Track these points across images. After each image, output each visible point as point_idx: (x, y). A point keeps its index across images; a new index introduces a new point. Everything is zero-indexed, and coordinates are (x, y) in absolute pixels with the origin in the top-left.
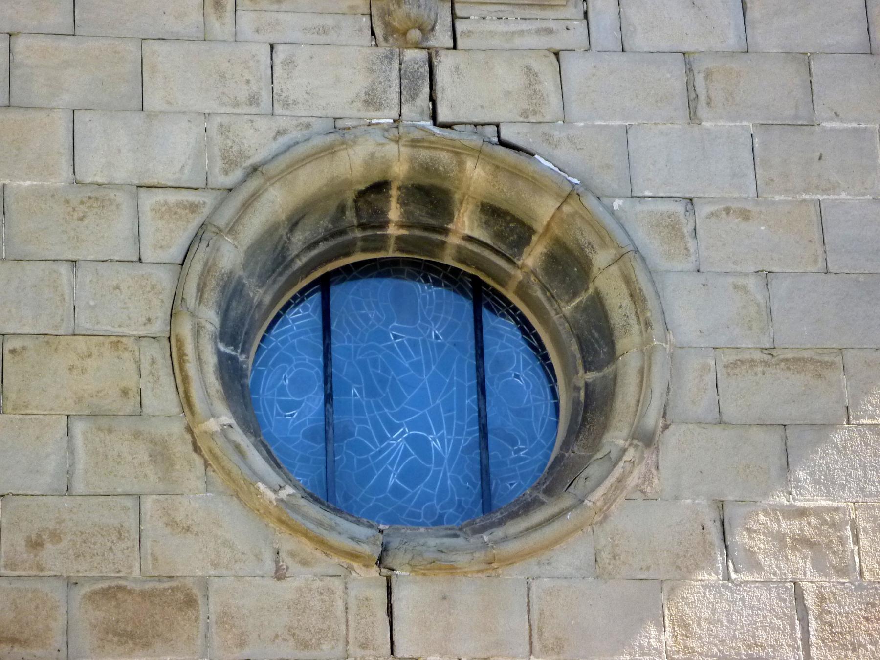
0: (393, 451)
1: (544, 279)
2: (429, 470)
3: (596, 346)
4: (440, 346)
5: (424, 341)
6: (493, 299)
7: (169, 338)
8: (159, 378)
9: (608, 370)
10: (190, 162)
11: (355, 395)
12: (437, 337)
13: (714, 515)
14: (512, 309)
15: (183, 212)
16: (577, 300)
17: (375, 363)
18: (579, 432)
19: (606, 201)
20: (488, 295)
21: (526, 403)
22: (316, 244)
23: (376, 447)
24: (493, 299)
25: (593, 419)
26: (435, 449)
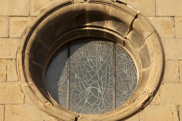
0: (88, 92)
1: (132, 42)
2: (97, 98)
3: (146, 61)
4: (102, 62)
5: (97, 61)
6: (119, 48)
7: (16, 59)
8: (12, 71)
9: (149, 68)
10: (25, 9)
11: (76, 77)
12: (101, 60)
13: (176, 109)
14: (124, 51)
15: (22, 23)
16: (141, 48)
17: (82, 67)
18: (140, 86)
19: (147, 17)
20: (118, 47)
21: (127, 79)
22: (64, 33)
23: (82, 92)
24: (119, 48)
25: (144, 82)
26: (99, 92)
